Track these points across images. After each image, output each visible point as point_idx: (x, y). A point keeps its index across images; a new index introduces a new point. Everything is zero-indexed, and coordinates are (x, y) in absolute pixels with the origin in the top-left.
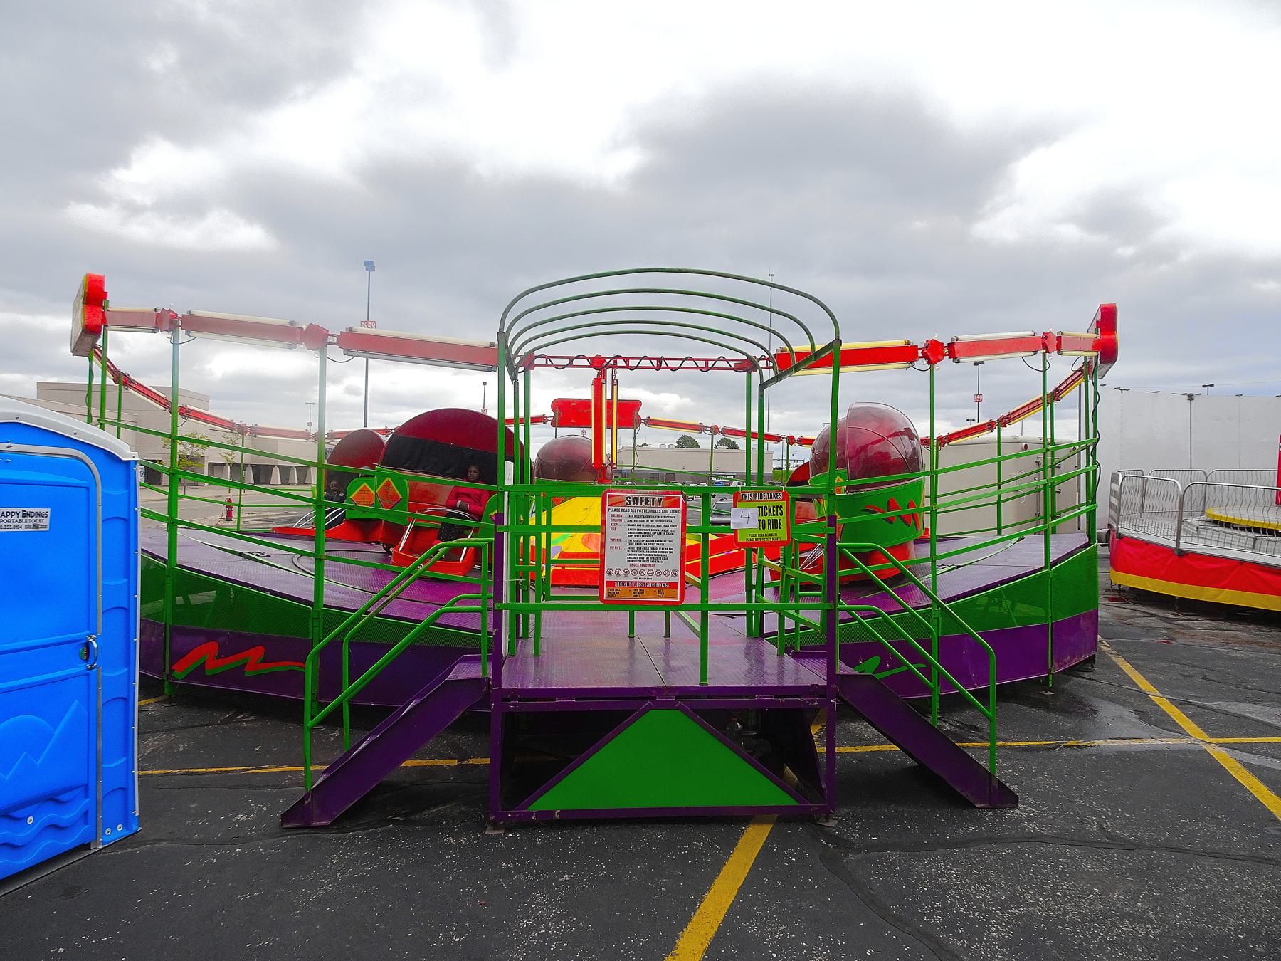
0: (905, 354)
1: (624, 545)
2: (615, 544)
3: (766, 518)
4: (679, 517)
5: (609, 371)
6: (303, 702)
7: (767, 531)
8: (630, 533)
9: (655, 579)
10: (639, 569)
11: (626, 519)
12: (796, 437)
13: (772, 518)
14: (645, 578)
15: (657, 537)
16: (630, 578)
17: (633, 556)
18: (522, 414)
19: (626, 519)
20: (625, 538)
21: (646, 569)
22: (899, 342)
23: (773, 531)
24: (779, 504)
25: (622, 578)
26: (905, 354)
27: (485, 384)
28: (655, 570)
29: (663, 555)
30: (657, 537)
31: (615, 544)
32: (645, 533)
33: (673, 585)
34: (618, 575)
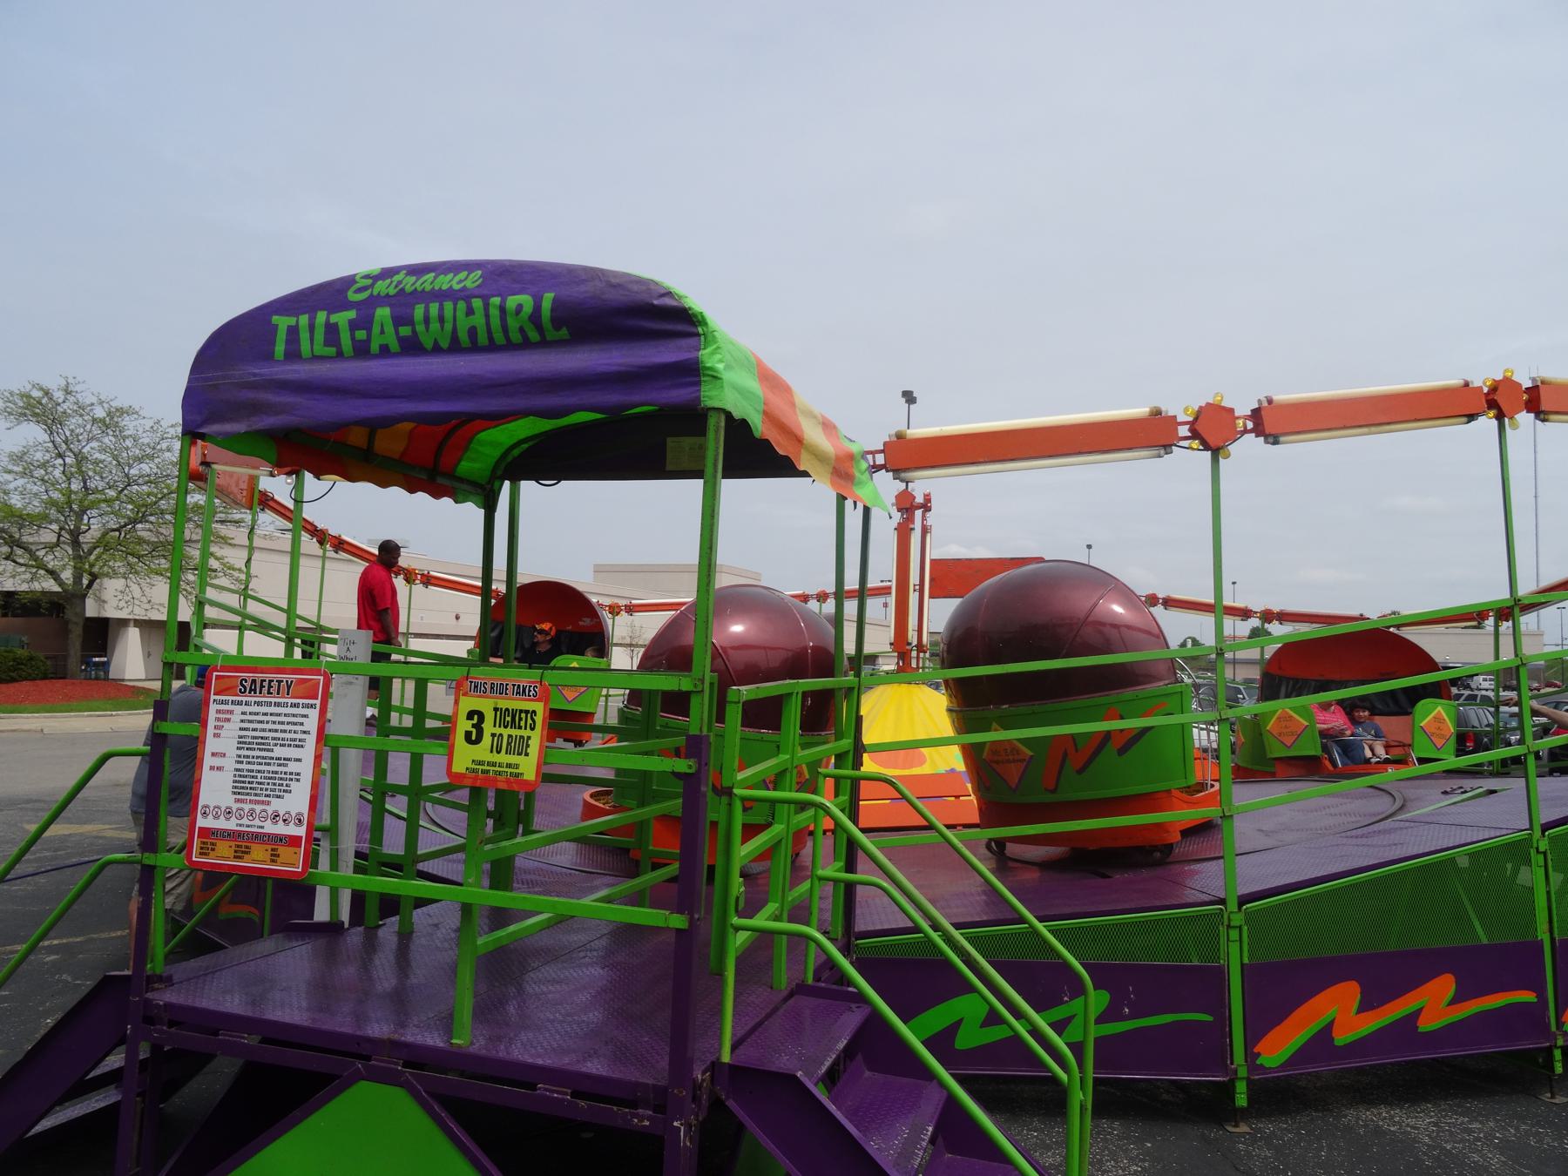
0: (1150, 434)
1: (229, 764)
2: (217, 762)
3: (506, 732)
4: (314, 714)
5: (918, 513)
6: (1097, 1067)
7: (503, 758)
8: (242, 743)
9: (269, 828)
10: (247, 807)
11: (236, 717)
12: (1160, 596)
13: (515, 732)
14: (255, 825)
15: (279, 752)
16: (232, 825)
17: (242, 786)
18: (851, 582)
19: (236, 717)
20: (232, 751)
21: (258, 808)
22: (1140, 411)
23: (513, 759)
24: (530, 706)
25: (221, 824)
26: (1150, 434)
27: (1089, 547)
28: (270, 809)
29: (281, 786)
30: (279, 752)
31: (217, 762)
32: (263, 744)
33: (294, 841)
34: (216, 817)
